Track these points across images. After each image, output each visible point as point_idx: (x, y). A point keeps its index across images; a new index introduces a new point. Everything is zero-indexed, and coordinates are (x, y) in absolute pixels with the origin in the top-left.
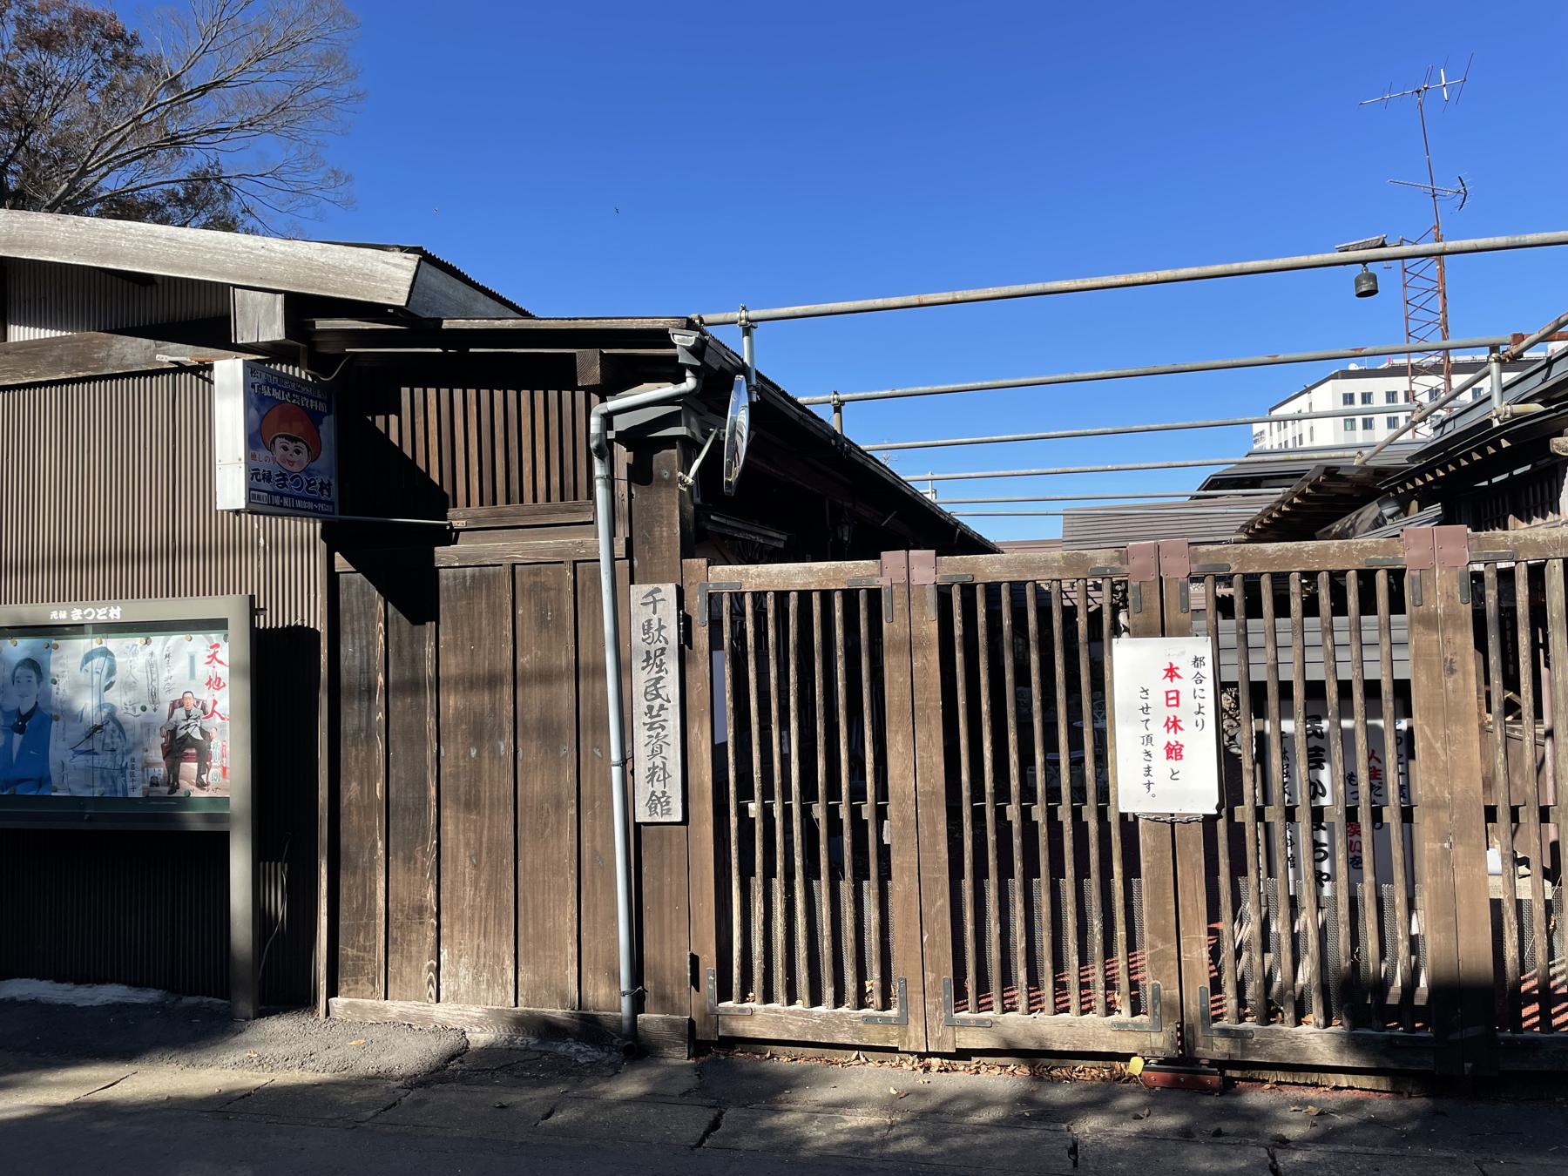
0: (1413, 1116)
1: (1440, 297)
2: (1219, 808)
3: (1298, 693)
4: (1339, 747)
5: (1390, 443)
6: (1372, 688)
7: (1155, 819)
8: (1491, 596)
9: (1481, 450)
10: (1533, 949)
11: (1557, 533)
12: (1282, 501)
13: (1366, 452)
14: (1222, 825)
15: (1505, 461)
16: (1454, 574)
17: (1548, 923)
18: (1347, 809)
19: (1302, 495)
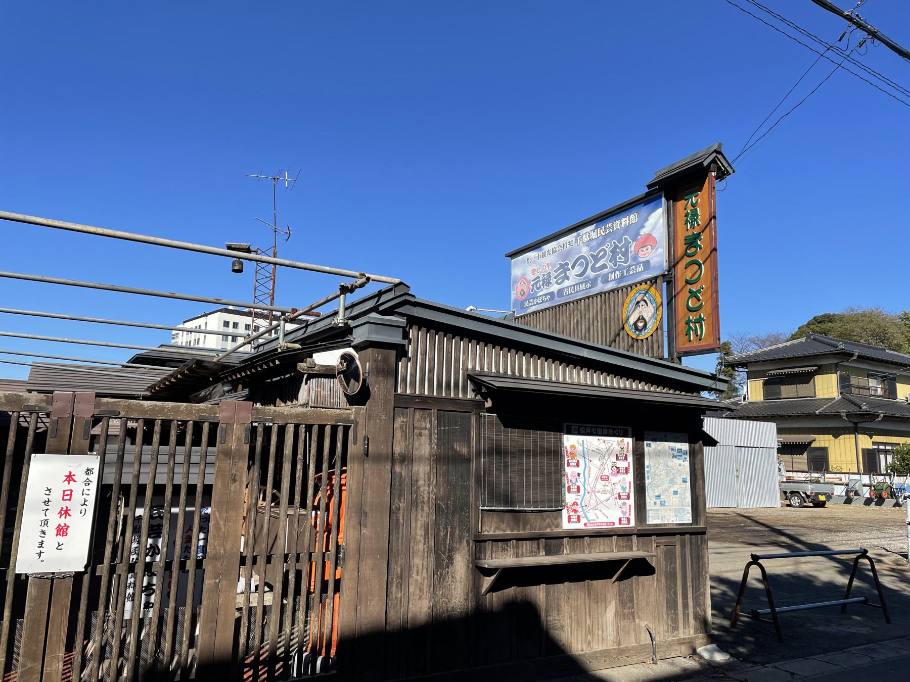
0: (721, 628)
1: (272, 282)
2: (86, 567)
3: (149, 492)
4: (168, 525)
5: (234, 351)
6: (192, 489)
7: (41, 577)
8: (259, 440)
9: (267, 364)
10: (254, 637)
11: (294, 410)
12: (171, 376)
13: (221, 355)
14: (86, 578)
15: (276, 371)
16: (243, 427)
17: (263, 620)
18: (166, 563)
19: (182, 374)
